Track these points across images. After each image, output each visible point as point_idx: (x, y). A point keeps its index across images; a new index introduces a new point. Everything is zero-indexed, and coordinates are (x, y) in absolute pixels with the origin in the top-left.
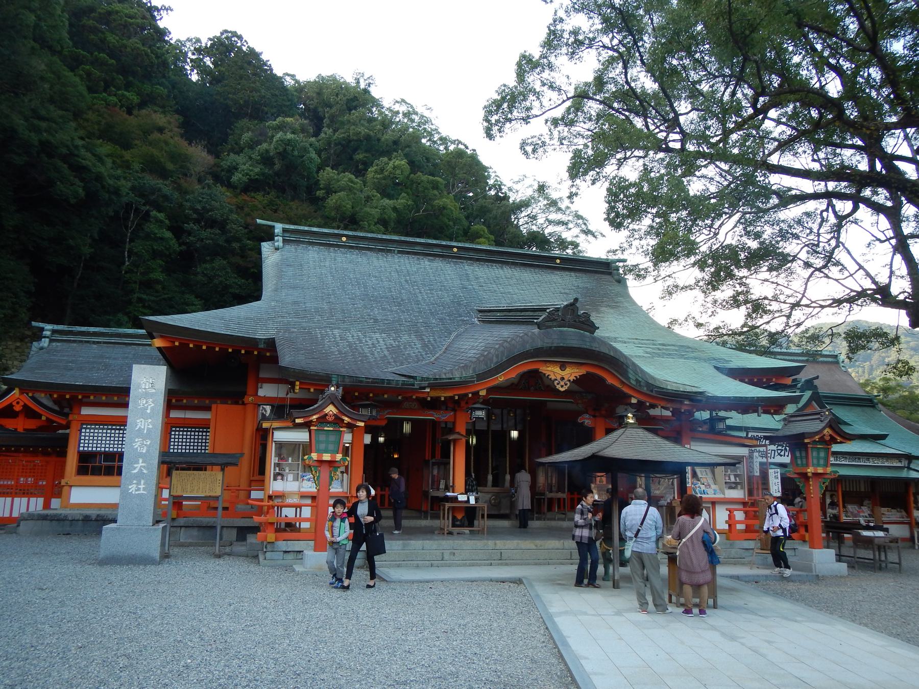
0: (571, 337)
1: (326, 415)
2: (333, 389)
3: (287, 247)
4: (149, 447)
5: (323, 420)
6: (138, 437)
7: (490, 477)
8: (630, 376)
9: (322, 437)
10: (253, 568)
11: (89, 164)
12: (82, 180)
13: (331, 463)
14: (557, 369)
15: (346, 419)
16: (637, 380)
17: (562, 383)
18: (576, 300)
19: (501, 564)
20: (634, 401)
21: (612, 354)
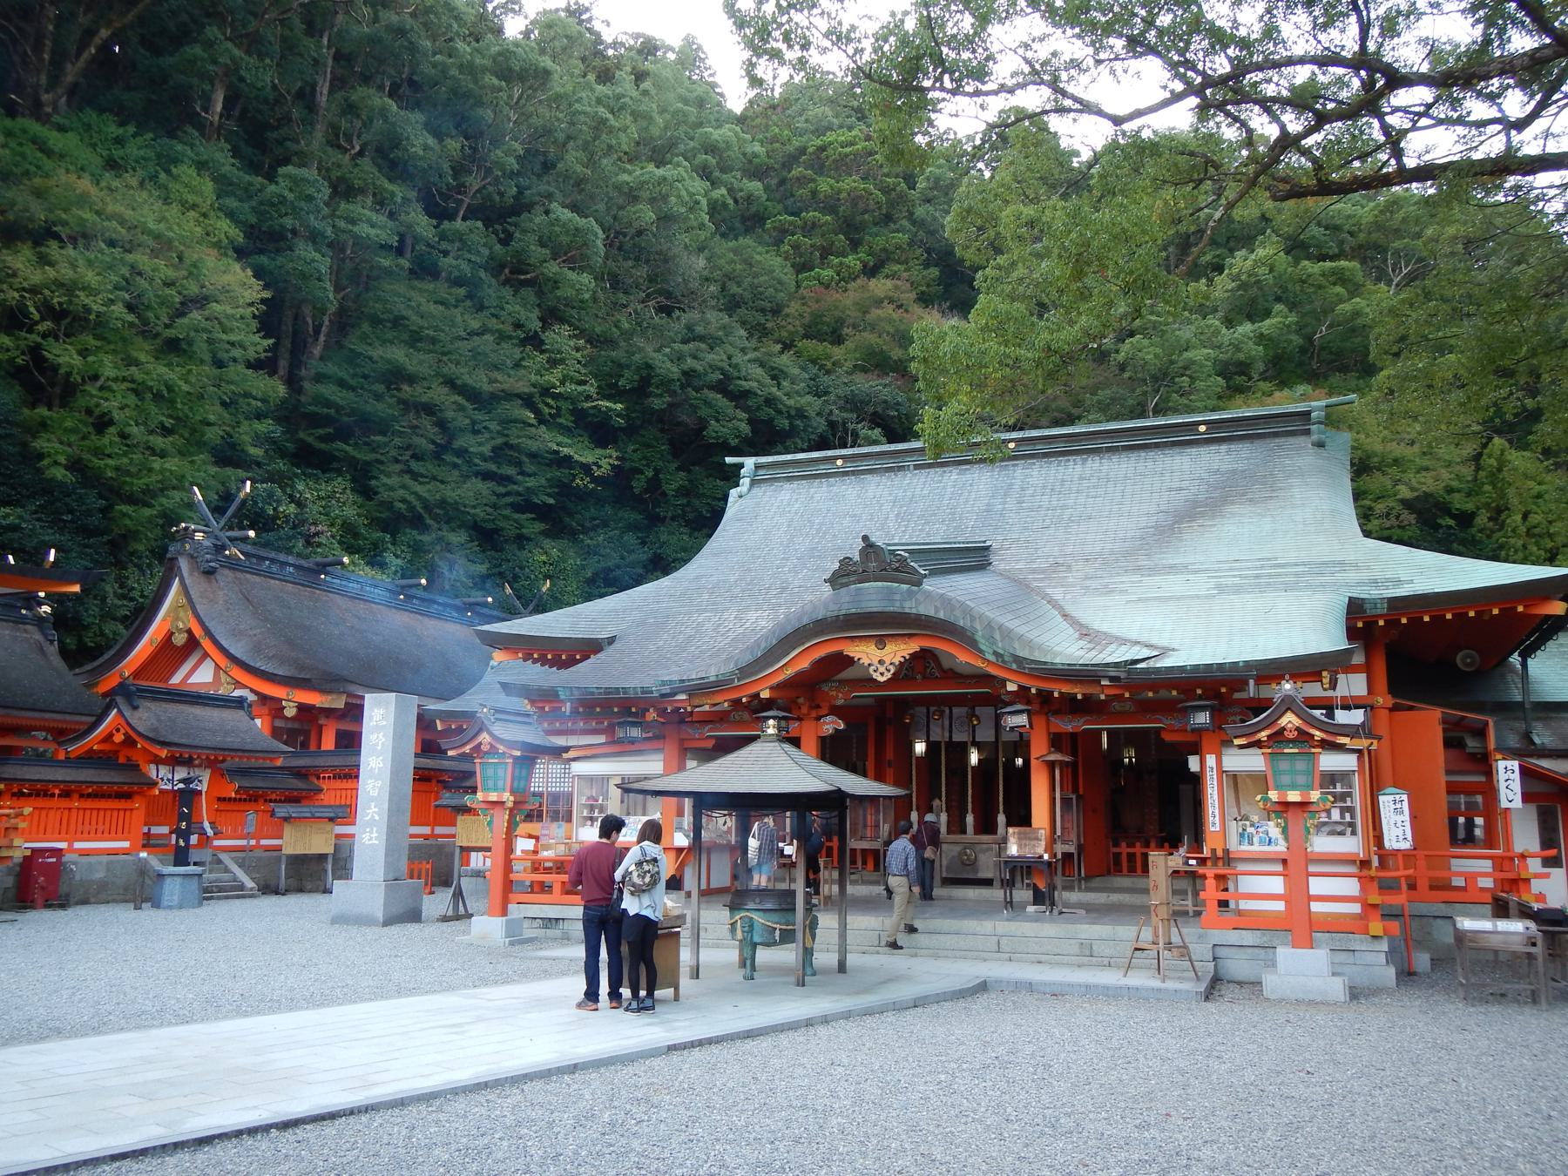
0: (873, 596)
1: (1284, 729)
5: (1278, 737)
7: (970, 819)
10: (148, 915)
11: (755, 384)
12: (746, 409)
13: (1303, 805)
15: (1318, 735)
16: (995, 653)
17: (882, 669)
18: (865, 538)
20: (1011, 687)
21: (941, 615)
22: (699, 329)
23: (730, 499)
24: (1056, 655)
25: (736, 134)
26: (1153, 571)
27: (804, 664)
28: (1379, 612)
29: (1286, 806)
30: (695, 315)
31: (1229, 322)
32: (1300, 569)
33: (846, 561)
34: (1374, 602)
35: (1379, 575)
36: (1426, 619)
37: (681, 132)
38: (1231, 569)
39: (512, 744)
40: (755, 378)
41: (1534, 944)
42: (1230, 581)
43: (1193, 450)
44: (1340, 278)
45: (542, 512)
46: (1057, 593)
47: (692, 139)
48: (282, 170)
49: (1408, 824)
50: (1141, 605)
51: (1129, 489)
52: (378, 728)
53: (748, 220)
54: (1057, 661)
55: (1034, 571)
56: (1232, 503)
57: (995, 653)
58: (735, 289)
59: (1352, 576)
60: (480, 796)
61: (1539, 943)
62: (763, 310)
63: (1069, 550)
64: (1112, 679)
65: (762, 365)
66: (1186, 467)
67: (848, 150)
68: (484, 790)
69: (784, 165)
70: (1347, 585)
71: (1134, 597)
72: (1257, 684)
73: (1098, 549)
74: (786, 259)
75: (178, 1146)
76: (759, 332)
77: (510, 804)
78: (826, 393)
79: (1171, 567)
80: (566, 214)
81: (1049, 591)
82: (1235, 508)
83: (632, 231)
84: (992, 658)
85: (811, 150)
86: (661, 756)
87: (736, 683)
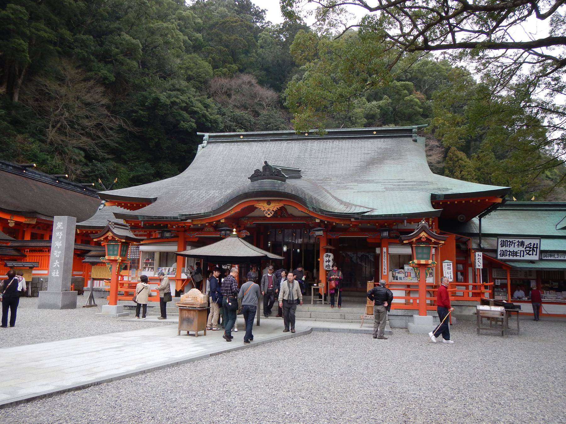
0: (267, 184)
1: (421, 237)
2: (423, 222)
3: (209, 146)
4: (60, 254)
5: (419, 241)
6: (56, 250)
8: (308, 206)
9: (420, 251)
11: (198, 109)
13: (425, 265)
14: (265, 205)
15: (433, 240)
16: (313, 208)
18: (266, 162)
19: (345, 322)
20: (318, 221)
21: (293, 193)
22: (177, 86)
23: (199, 148)
24: (336, 209)
25: (192, 14)
26: (362, 182)
27: (239, 210)
28: (441, 199)
29: (420, 265)
30: (175, 81)
31: (369, 100)
32: (413, 183)
33: (257, 171)
34: (439, 196)
35: (440, 186)
36: (449, 203)
37: (169, 12)
38: (389, 182)
39: (121, 237)
40: (198, 106)
41: (503, 315)
42: (389, 186)
43: (372, 140)
44: (406, 87)
45: (112, 151)
46: (328, 188)
47: (174, 14)
48: (9, 5)
49: (452, 273)
50: (359, 193)
51: (350, 152)
52: (59, 230)
53: (197, 47)
54: (336, 211)
55: (318, 180)
56: (387, 159)
57: (313, 208)
58: (190, 73)
59: (431, 187)
60: (107, 257)
61: (505, 315)
62: (200, 82)
63: (330, 173)
64: (355, 219)
65: (201, 102)
66: (369, 146)
67: (234, 24)
68: (109, 255)
69: (209, 28)
70: (430, 189)
71: (356, 191)
72: (407, 222)
73: (341, 173)
74: (210, 63)
75: (18, 403)
76: (198, 89)
77: (120, 261)
78: (225, 115)
79: (368, 181)
80: (127, 37)
81: (325, 187)
82: (388, 161)
83: (152, 46)
84: (311, 210)
85: (220, 23)
86: (176, 244)
87: (212, 216)
